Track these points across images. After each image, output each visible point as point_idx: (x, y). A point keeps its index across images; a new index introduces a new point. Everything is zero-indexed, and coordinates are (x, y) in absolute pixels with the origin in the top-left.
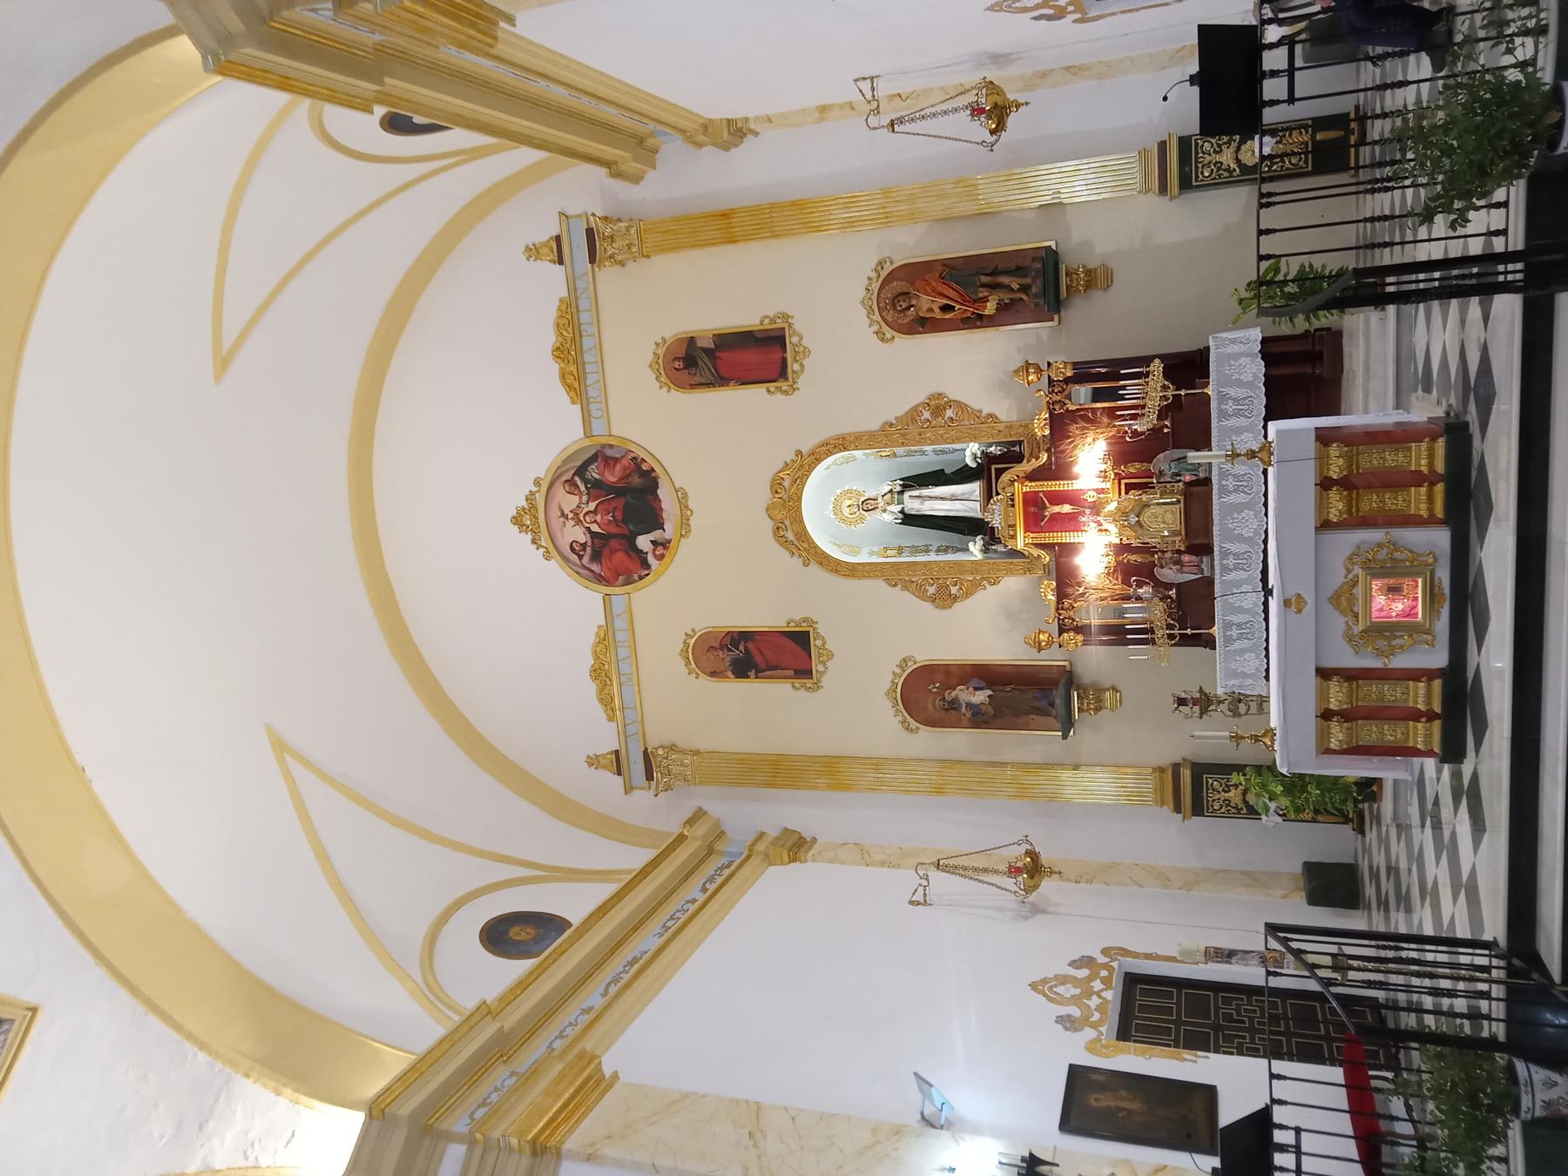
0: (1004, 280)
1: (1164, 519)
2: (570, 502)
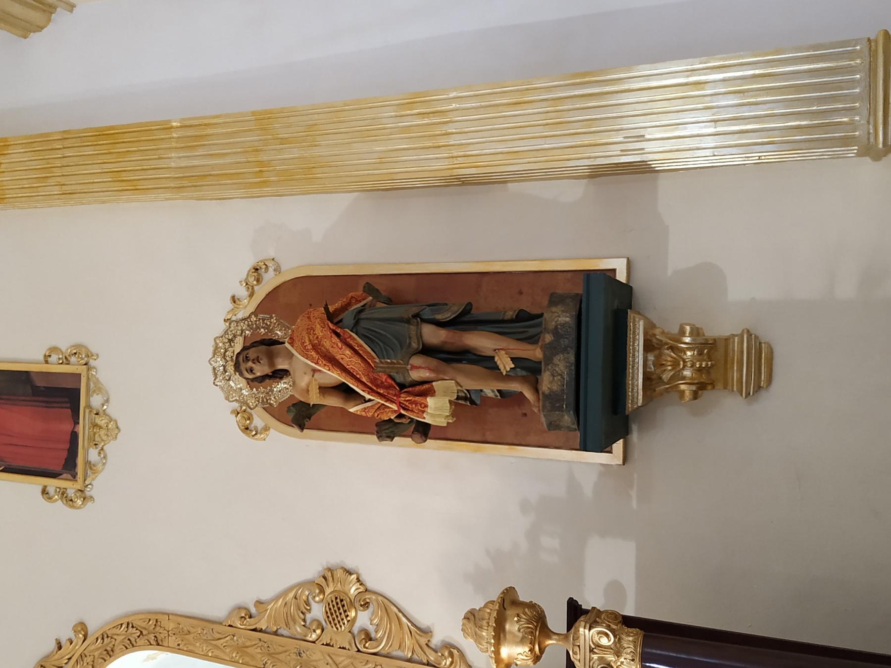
0: (481, 341)
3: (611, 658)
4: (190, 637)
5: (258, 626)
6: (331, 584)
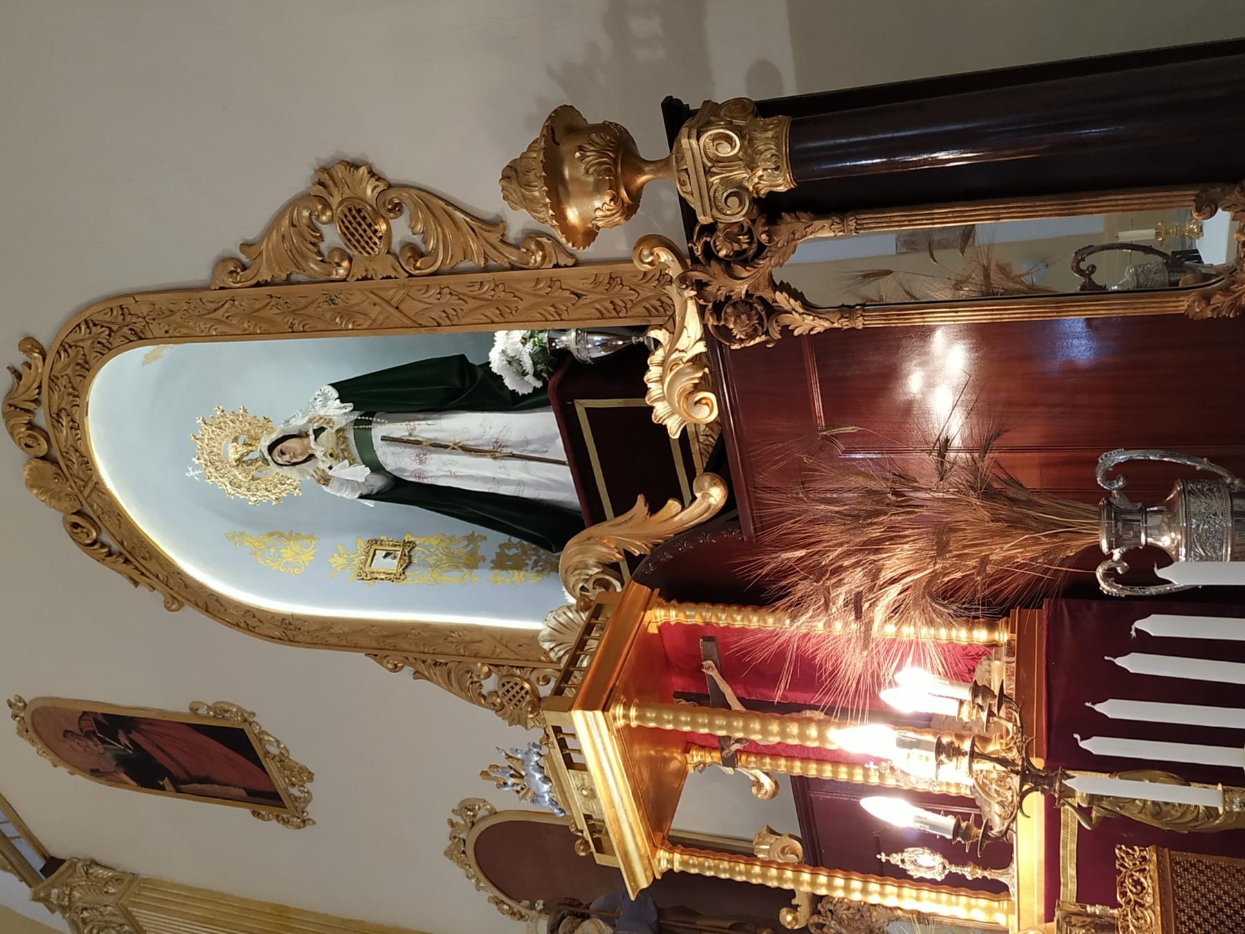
3: (740, 174)
4: (176, 318)
5: (261, 278)
6: (335, 191)
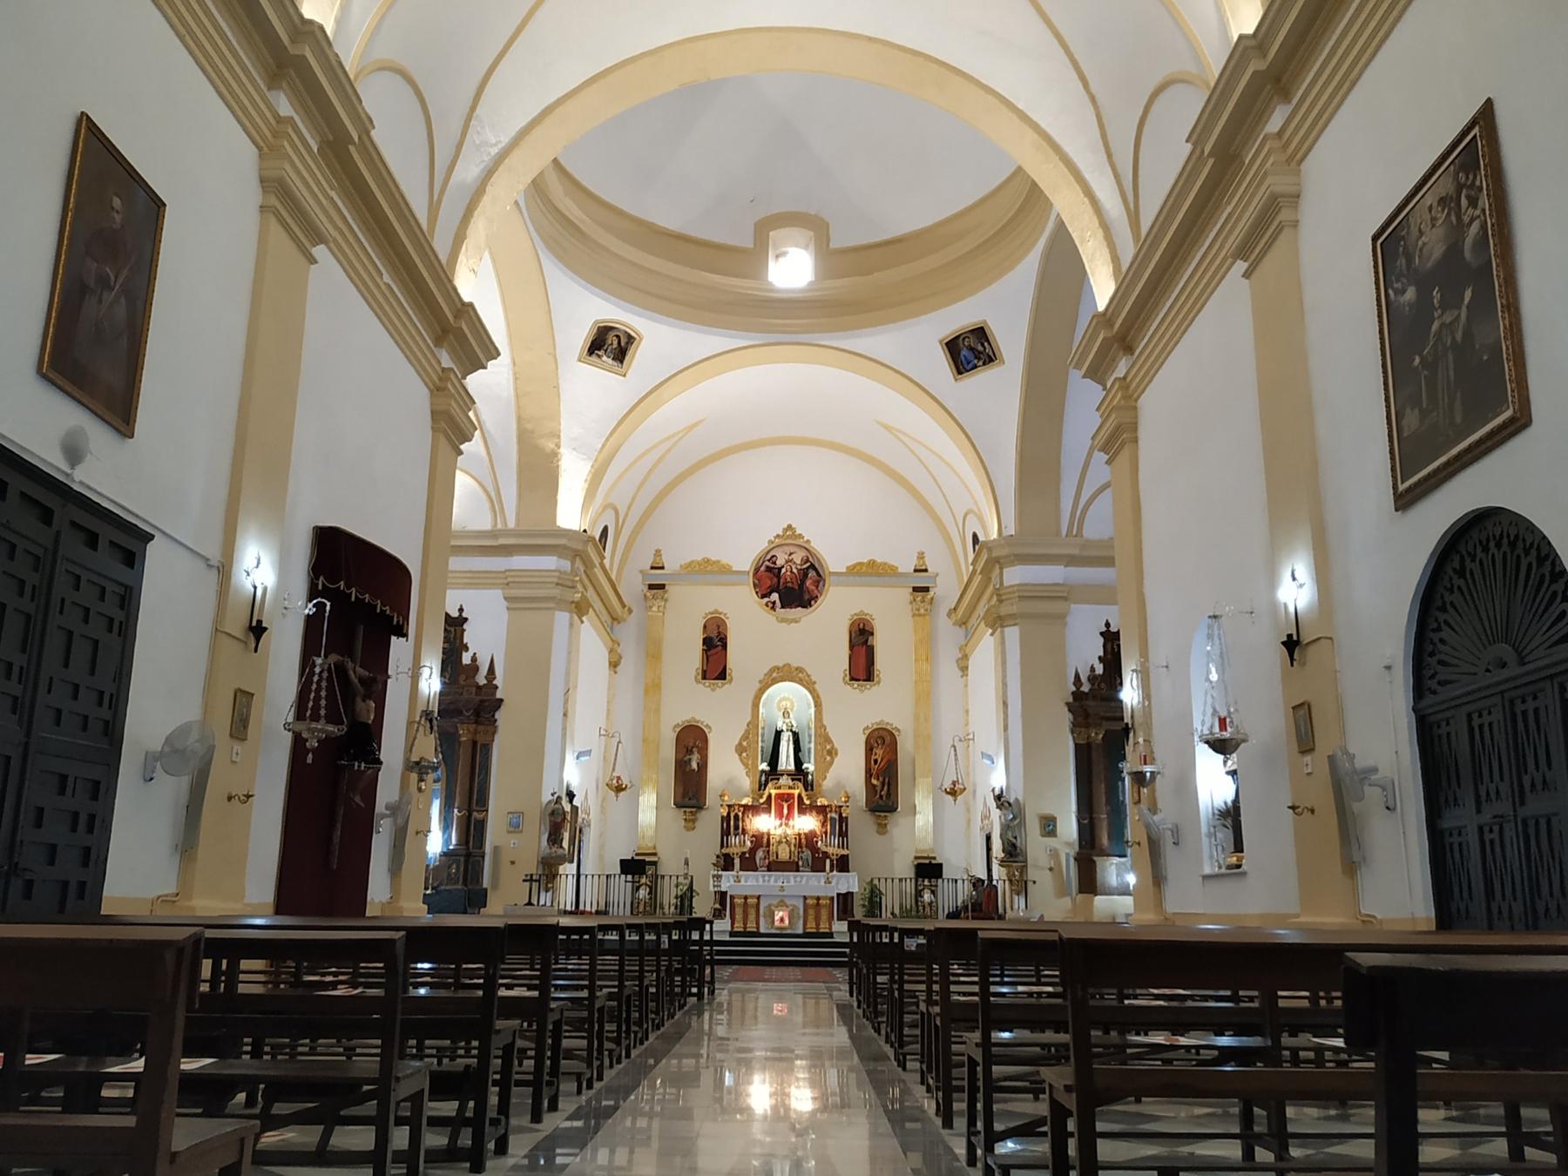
1: (784, 854)
2: (798, 558)
